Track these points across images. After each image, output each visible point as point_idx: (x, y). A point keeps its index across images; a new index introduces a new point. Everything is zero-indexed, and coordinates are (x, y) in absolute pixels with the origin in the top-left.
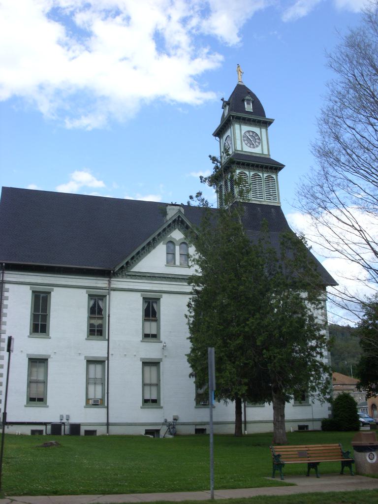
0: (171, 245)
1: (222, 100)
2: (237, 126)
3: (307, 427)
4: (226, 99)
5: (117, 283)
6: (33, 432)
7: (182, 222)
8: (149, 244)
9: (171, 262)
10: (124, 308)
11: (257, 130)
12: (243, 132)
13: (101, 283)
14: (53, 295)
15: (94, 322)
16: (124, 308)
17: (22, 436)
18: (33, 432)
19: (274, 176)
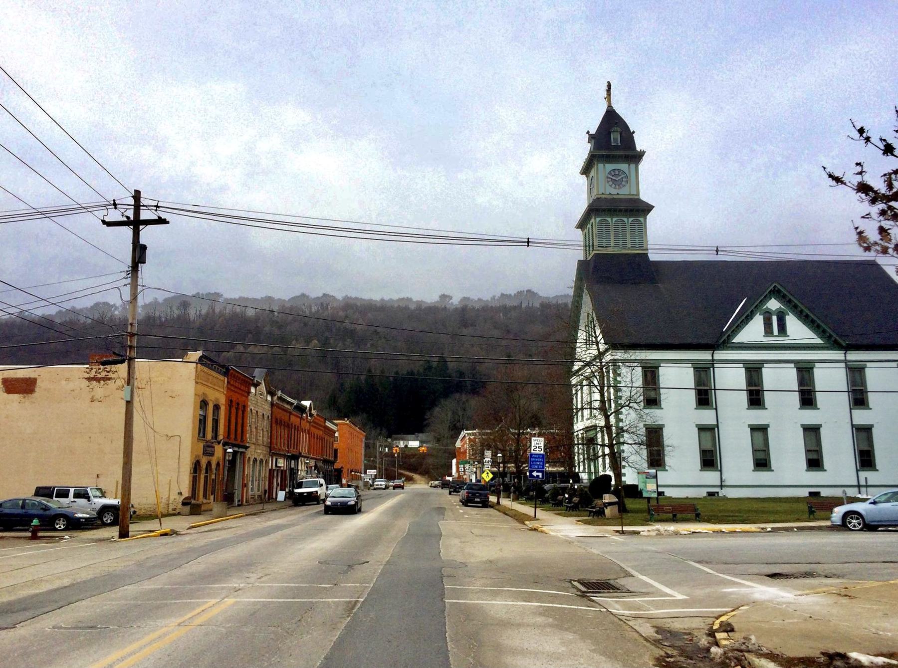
0: (767, 315)
1: (588, 132)
2: (601, 166)
3: (819, 493)
4: (593, 132)
5: (720, 355)
6: (810, 493)
7: (779, 291)
8: (807, 316)
9: (768, 331)
10: (730, 377)
11: (623, 167)
12: (607, 171)
13: (705, 356)
14: (765, 371)
15: (235, 397)
16: (730, 377)
17: (797, 500)
18: (810, 493)
19: (642, 219)
